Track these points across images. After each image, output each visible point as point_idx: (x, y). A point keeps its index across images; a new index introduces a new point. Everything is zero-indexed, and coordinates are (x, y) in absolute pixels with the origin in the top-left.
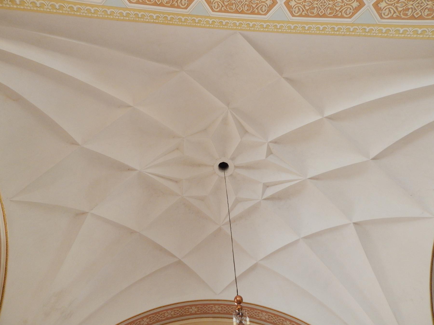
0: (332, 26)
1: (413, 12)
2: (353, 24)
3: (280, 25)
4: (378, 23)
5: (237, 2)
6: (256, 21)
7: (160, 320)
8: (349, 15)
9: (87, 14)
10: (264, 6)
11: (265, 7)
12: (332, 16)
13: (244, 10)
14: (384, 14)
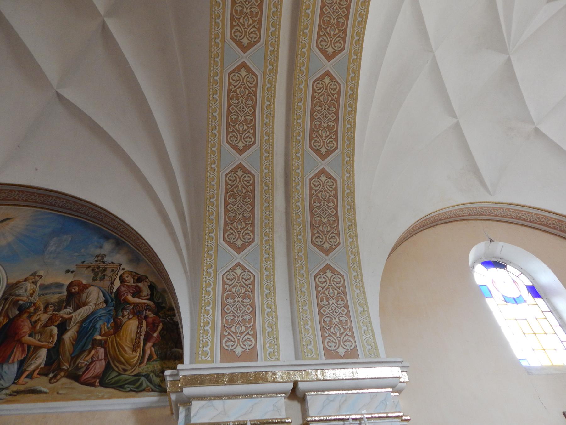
0: (221, 35)
1: (235, 105)
2: (223, 41)
3: (216, 133)
4: (224, 71)
5: (241, 313)
6: (217, 206)
7: (15, 299)
8: (233, 36)
9: (203, 321)
10: (234, 344)
11: (233, 345)
12: (233, 13)
13: (235, 5)
14: (234, 76)
